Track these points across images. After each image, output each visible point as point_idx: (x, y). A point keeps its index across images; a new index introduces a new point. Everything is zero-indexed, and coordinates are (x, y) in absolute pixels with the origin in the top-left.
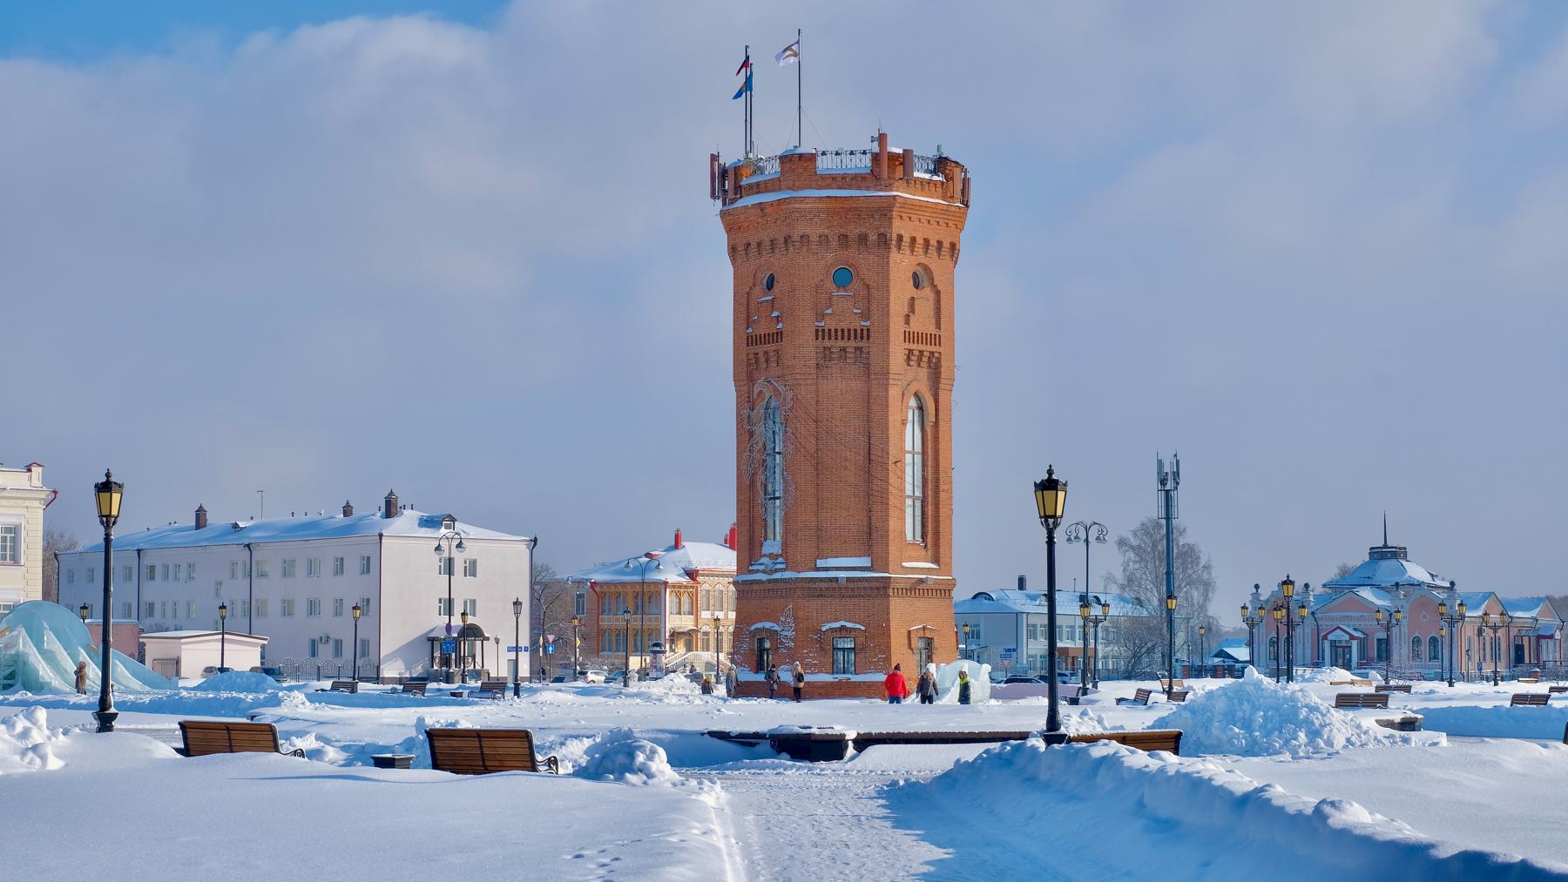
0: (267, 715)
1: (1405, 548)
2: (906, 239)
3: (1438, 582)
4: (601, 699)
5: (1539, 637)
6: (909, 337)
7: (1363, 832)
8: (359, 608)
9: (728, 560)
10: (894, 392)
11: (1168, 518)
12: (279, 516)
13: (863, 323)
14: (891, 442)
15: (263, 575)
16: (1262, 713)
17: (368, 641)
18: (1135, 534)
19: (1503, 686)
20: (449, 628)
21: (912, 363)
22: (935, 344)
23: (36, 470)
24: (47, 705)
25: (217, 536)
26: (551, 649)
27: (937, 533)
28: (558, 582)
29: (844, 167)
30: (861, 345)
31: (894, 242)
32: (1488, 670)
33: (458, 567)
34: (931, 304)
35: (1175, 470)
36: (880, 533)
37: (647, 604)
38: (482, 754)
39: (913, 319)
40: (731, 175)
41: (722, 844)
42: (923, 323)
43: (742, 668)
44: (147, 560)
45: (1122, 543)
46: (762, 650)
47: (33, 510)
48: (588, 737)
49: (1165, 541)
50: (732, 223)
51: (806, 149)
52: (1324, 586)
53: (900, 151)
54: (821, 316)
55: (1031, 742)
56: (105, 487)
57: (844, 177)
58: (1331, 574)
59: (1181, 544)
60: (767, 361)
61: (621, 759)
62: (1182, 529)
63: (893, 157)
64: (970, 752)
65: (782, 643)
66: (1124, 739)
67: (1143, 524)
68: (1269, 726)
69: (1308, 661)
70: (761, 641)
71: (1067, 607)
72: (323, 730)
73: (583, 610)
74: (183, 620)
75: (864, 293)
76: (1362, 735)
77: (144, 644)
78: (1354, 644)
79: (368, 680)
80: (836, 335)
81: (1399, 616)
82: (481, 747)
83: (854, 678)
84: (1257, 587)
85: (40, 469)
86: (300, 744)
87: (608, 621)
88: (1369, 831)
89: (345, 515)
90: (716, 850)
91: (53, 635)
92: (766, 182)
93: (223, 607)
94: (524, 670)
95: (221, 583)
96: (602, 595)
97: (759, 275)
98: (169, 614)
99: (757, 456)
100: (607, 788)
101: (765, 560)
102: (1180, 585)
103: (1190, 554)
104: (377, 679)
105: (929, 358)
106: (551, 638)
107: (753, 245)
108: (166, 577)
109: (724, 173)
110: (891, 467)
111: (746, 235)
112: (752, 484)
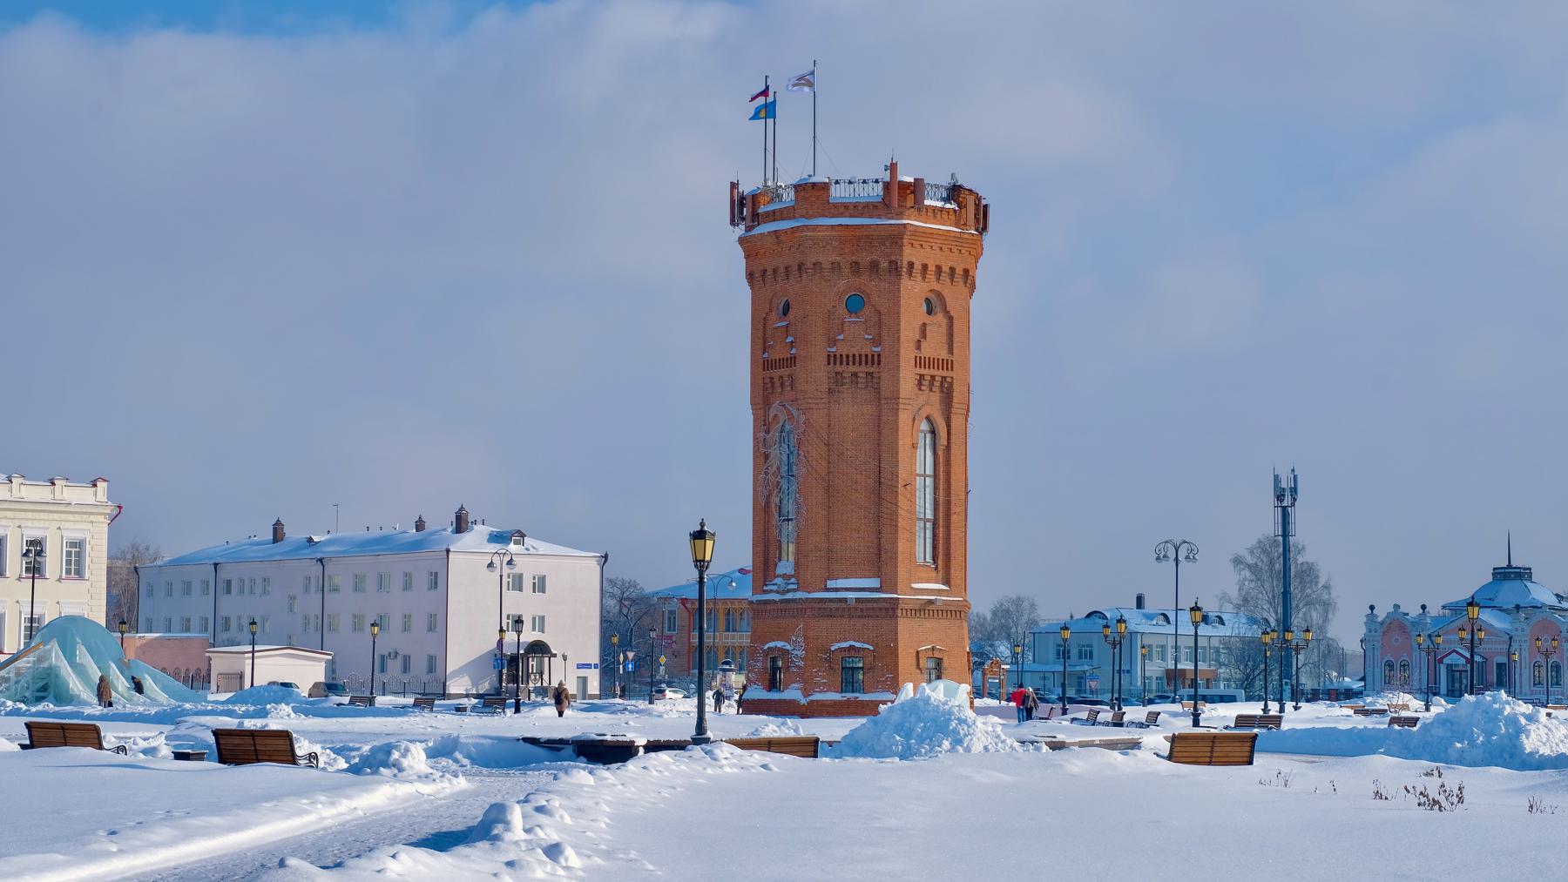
1: (1530, 569)
2: (918, 266)
6: (919, 362)
8: (377, 625)
10: (904, 417)
11: (1285, 535)
12: (354, 530)
13: (874, 349)
16: (922, 724)
17: (436, 657)
18: (1251, 552)
21: (923, 388)
22: (947, 369)
23: (102, 486)
25: (291, 550)
26: (630, 666)
27: (948, 555)
29: (857, 195)
30: (872, 370)
31: (904, 270)
34: (944, 329)
35: (1293, 486)
36: (889, 555)
37: (738, 621)
38: (256, 750)
39: (924, 345)
40: (749, 203)
42: (934, 348)
43: (756, 686)
44: (224, 574)
46: (775, 669)
47: (98, 525)
48: (421, 742)
49: (1282, 559)
51: (819, 178)
52: (1444, 607)
53: (910, 180)
54: (833, 342)
57: (856, 205)
59: (1299, 562)
60: (782, 385)
61: (381, 756)
62: (1300, 547)
63: (904, 186)
65: (793, 662)
67: (1260, 542)
68: (924, 735)
70: (774, 660)
73: (675, 626)
76: (1000, 744)
77: (210, 659)
80: (860, 359)
82: (255, 744)
83: (862, 697)
84: (1372, 608)
85: (105, 484)
89: (418, 530)
91: (84, 649)
92: (781, 210)
93: (254, 623)
95: (295, 598)
97: (775, 300)
99: (771, 478)
101: (778, 581)
102: (1297, 606)
103: (1309, 573)
105: (942, 382)
107: (770, 272)
108: (242, 591)
109: (742, 199)
110: (901, 489)
111: (762, 261)
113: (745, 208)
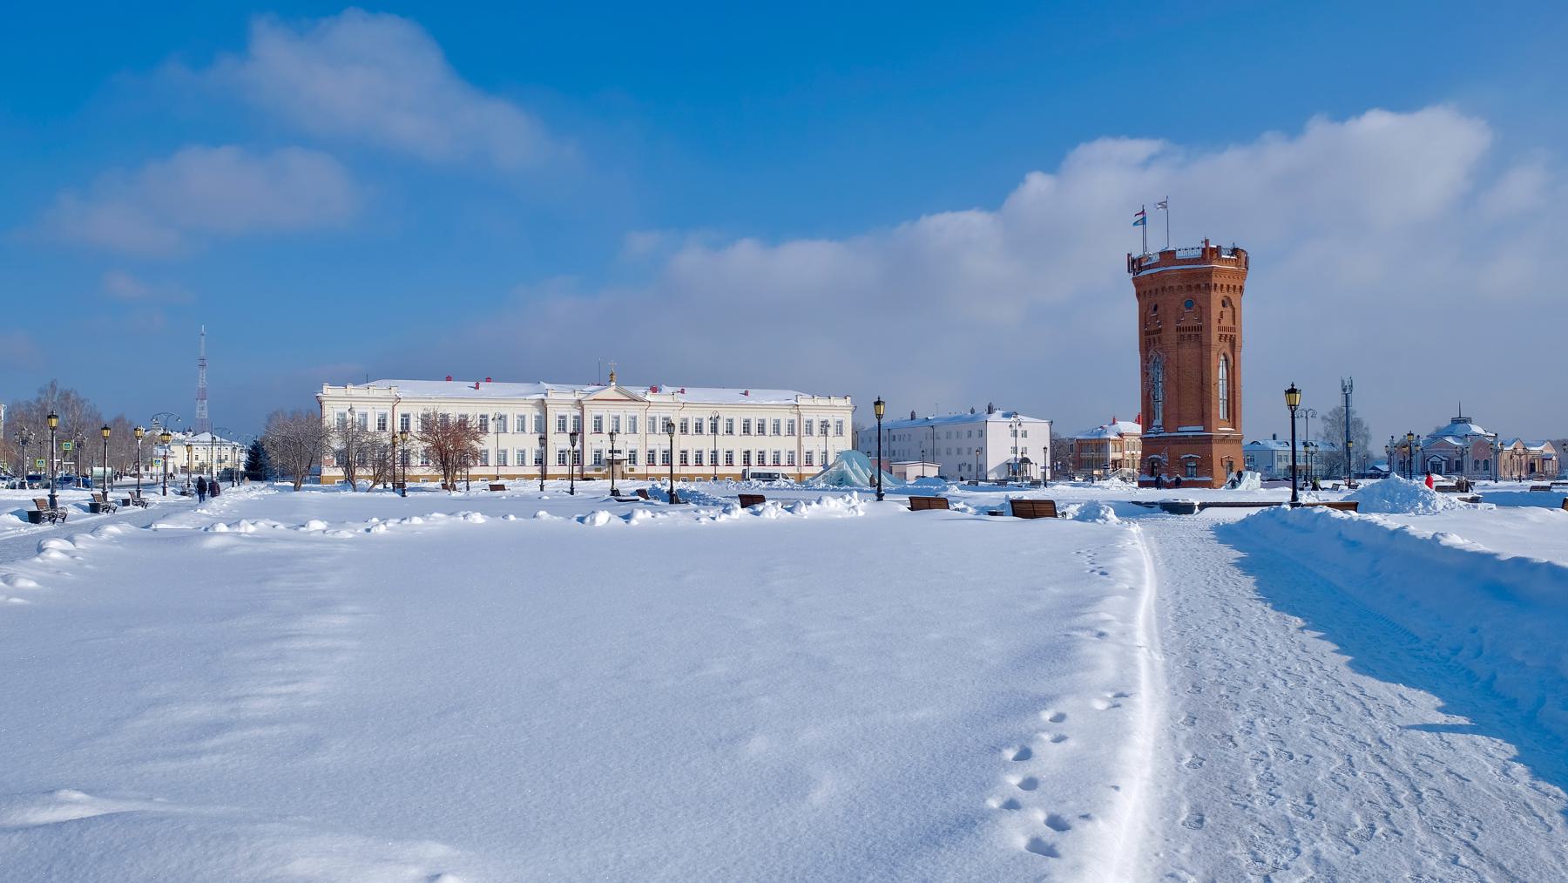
0: (943, 495)
2: (1219, 285)
3: (1489, 434)
4: (1082, 488)
5: (1544, 460)
6: (1220, 329)
7: (1459, 547)
9: (1138, 429)
10: (1214, 354)
14: (1213, 375)
15: (939, 438)
19: (1524, 483)
20: (1016, 459)
24: (858, 491)
28: (1061, 439)
32: (1515, 475)
33: (1019, 434)
34: (1231, 314)
35: (1291, 464)
40: (1137, 261)
41: (1141, 549)
44: (892, 433)
45: (1324, 418)
46: (1153, 467)
50: (1138, 283)
55: (1283, 506)
56: (878, 403)
58: (1431, 430)
60: (1155, 342)
61: (1094, 513)
63: (1212, 249)
64: (1254, 511)
66: (1330, 505)
69: (1419, 471)
70: (1153, 463)
71: (1300, 448)
72: (966, 500)
74: (907, 457)
75: (1199, 310)
78: (1443, 463)
79: (982, 481)
81: (1468, 450)
83: (1196, 479)
84: (1392, 437)
86: (958, 506)
87: (1084, 455)
88: (1462, 547)
89: (972, 413)
90: (1139, 551)
94: (1048, 477)
96: (1082, 445)
98: (901, 454)
100: (1088, 525)
103: (1359, 422)
104: (986, 481)
106: (1059, 463)
108: (900, 440)
109: (1134, 261)
112: (1148, 395)
113: (1135, 265)
